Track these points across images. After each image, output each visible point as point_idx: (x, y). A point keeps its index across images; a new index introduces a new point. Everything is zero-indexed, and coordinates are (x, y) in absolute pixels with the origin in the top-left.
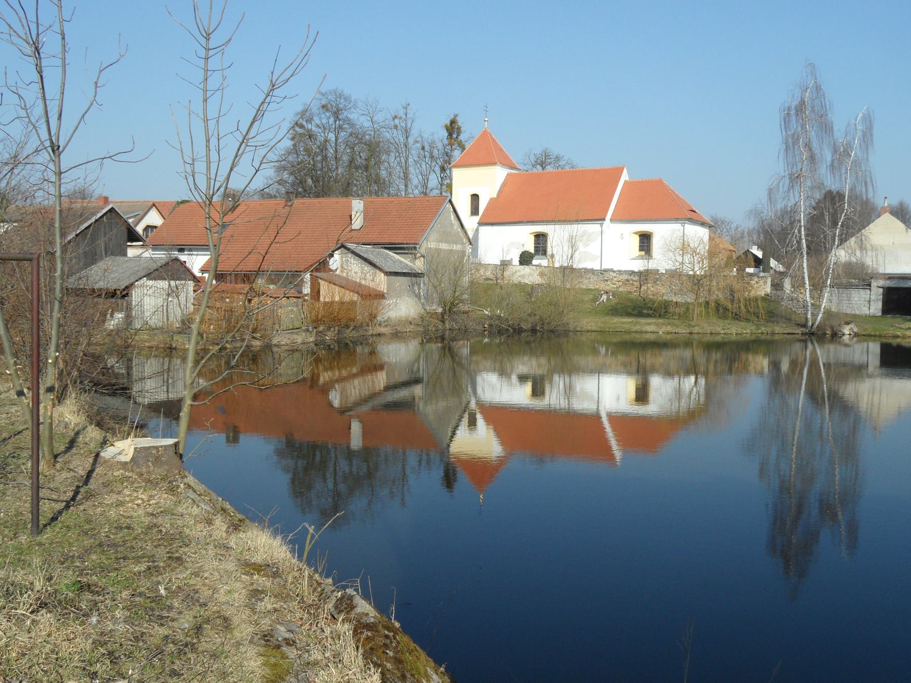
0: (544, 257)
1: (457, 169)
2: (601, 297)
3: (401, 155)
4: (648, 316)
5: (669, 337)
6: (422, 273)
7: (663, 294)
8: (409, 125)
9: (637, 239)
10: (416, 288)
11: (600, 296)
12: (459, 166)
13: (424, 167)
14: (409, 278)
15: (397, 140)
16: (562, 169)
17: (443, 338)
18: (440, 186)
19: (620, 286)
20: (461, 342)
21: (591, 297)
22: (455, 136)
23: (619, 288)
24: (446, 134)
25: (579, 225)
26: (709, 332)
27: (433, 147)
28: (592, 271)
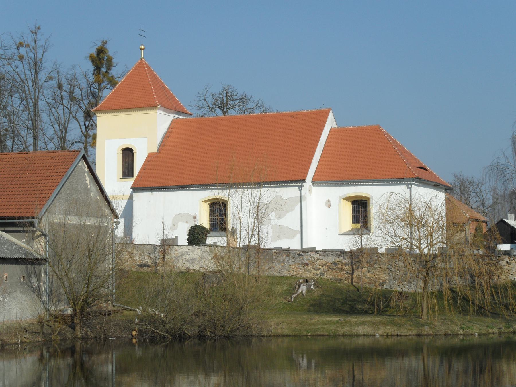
0: (223, 233)
1: (102, 115)
2: (299, 287)
3: (29, 97)
4: (365, 312)
5: (389, 341)
6: (42, 259)
7: (384, 282)
8: (39, 56)
9: (348, 208)
10: (34, 280)
11: (297, 287)
12: (107, 110)
13: (61, 112)
14: (23, 267)
15: (23, 77)
16: (250, 113)
17: (72, 351)
18: (83, 138)
19: (325, 272)
20: (103, 356)
21: (285, 287)
22: (104, 70)
23: (324, 274)
24: (91, 67)
25: (263, 190)
26: (443, 332)
27: (74, 86)
28: (287, 252)
